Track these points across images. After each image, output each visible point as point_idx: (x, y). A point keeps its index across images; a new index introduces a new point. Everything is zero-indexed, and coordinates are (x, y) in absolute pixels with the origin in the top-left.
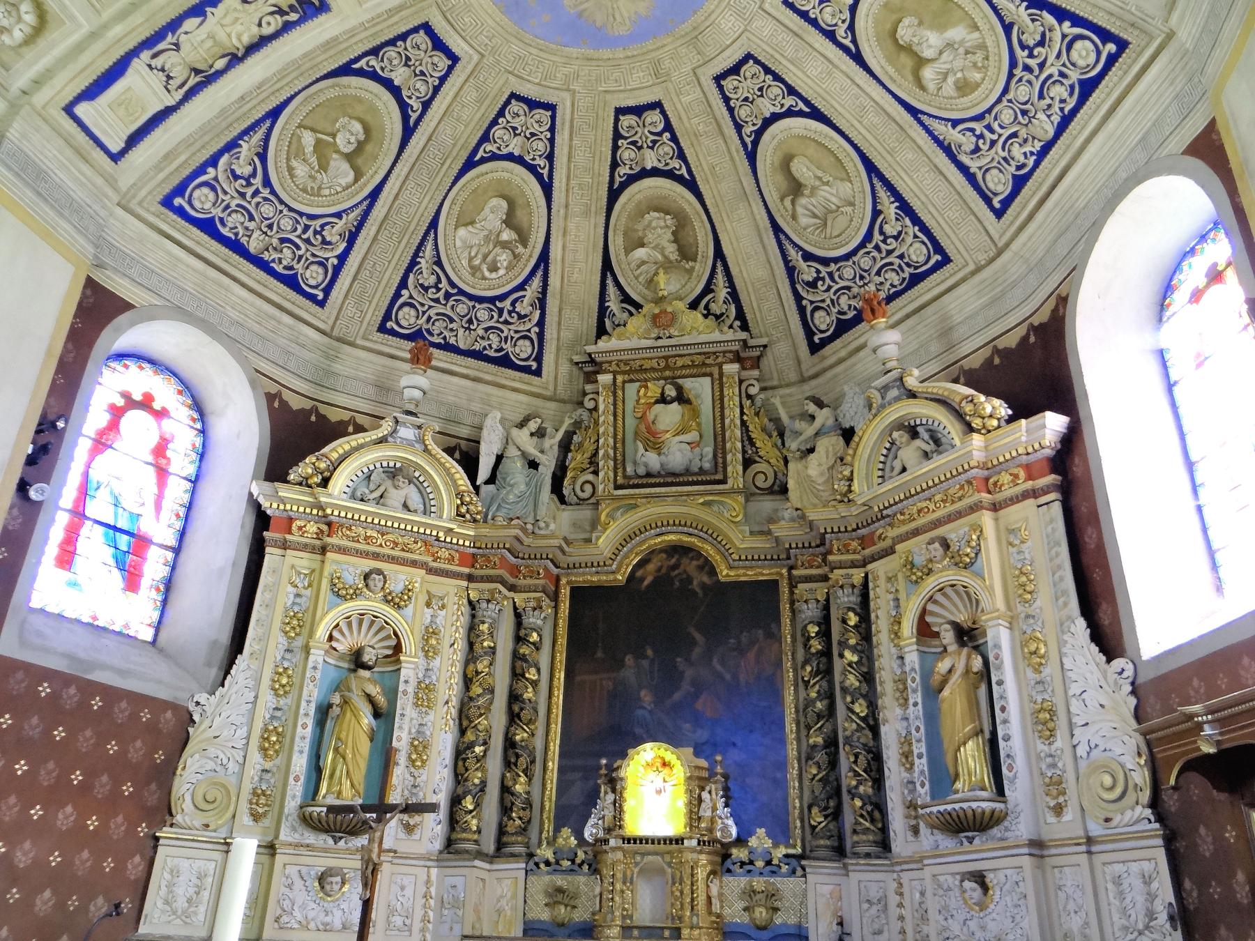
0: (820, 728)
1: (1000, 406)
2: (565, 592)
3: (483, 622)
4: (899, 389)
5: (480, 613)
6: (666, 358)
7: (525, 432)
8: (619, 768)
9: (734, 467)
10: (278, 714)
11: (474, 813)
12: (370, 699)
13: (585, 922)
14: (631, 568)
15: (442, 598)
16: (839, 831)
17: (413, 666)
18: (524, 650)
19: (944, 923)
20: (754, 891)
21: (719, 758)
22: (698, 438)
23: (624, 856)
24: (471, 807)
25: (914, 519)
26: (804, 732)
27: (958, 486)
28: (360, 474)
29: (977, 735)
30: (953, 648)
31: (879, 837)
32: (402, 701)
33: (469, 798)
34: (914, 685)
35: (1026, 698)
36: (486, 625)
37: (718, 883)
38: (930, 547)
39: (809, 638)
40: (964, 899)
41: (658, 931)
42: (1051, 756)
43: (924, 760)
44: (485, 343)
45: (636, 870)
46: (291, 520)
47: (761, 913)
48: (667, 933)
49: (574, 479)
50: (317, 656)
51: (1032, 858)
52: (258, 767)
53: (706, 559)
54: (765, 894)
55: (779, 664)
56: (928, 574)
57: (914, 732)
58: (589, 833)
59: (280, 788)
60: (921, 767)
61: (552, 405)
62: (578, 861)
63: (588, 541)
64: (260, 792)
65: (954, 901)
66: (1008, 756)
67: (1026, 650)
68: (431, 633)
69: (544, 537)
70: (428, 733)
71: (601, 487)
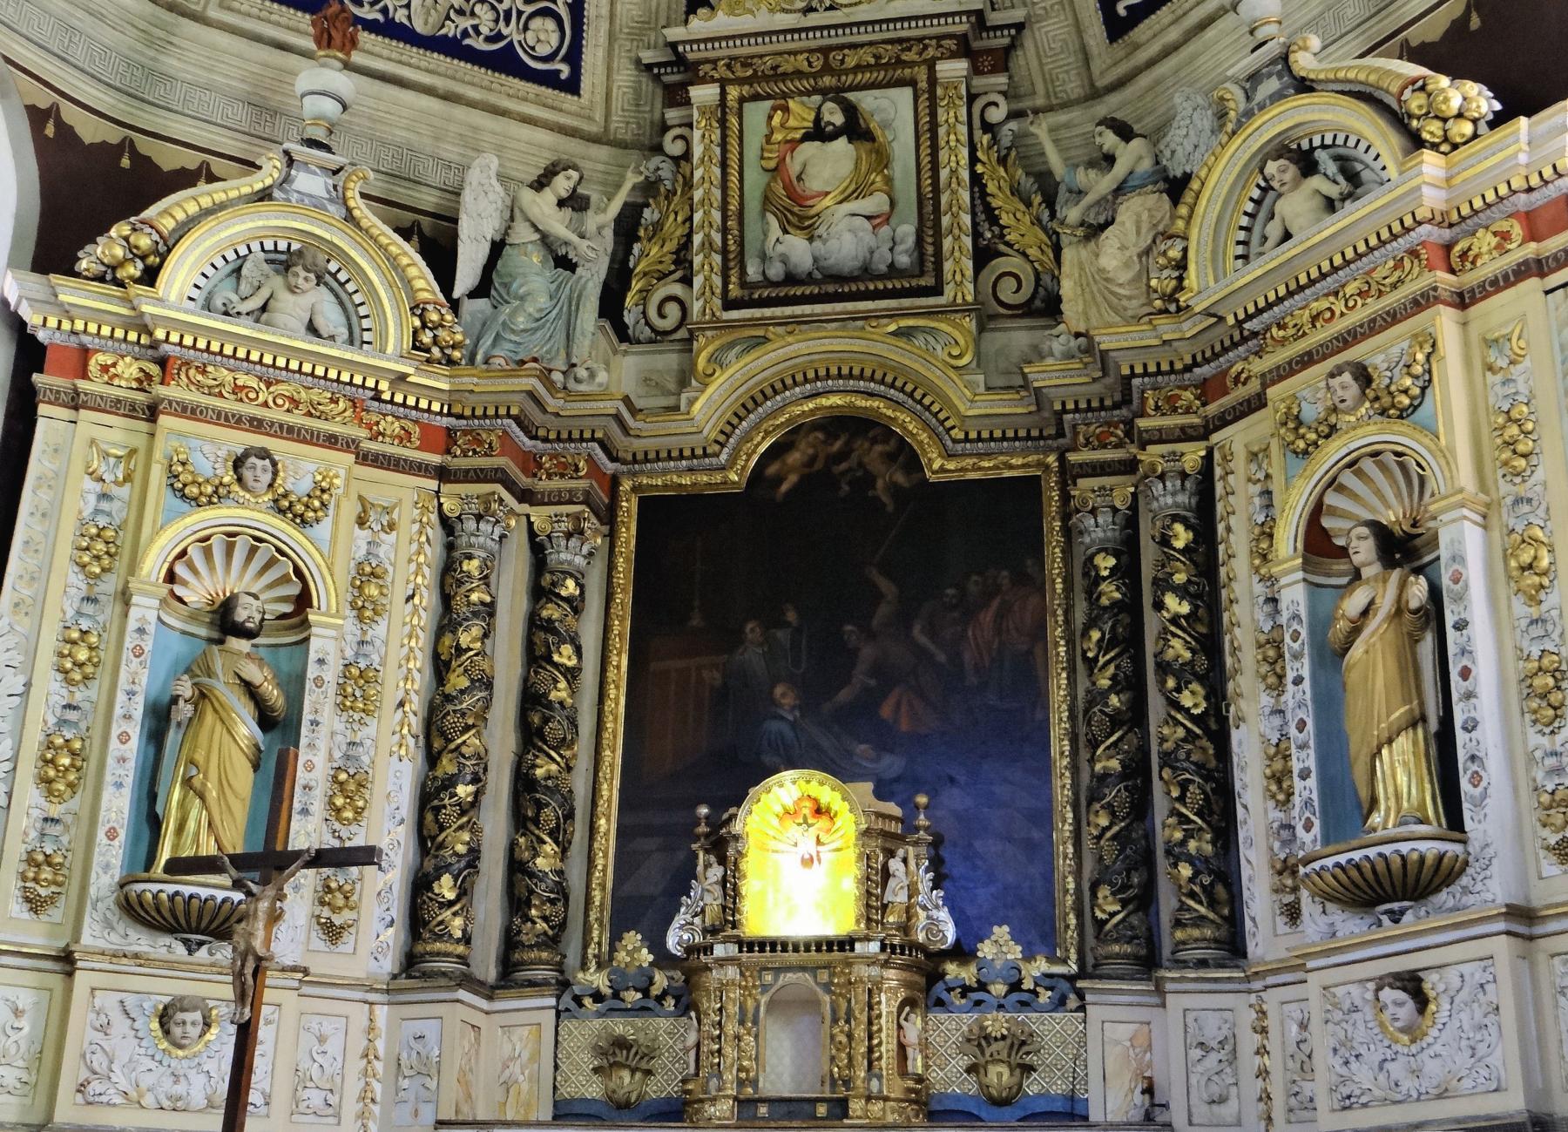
0: (1115, 744)
1: (1479, 94)
2: (629, 507)
3: (470, 557)
4: (1280, 76)
5: (464, 539)
6: (825, 51)
7: (549, 197)
8: (733, 817)
9: (957, 262)
10: (72, 715)
11: (457, 907)
12: (250, 690)
13: (669, 1099)
14: (755, 458)
15: (387, 510)
16: (1149, 929)
17: (333, 633)
18: (550, 611)
19: (1344, 1071)
20: (987, 1038)
21: (922, 800)
22: (886, 208)
23: (742, 974)
24: (450, 895)
25: (1305, 334)
26: (1084, 755)
27: (1391, 263)
28: (220, 263)
29: (1414, 725)
30: (1371, 571)
31: (1223, 933)
32: (314, 697)
33: (447, 880)
34: (1296, 646)
35: (1510, 654)
36: (475, 563)
37: (919, 1021)
38: (1335, 382)
39: (1099, 580)
40: (1382, 1025)
41: (806, 1107)
42: (1555, 754)
43: (1312, 782)
44: (466, 23)
45: (764, 1000)
46: (85, 353)
47: (1000, 1075)
48: (822, 1110)
49: (645, 293)
50: (145, 608)
51: (1512, 939)
52: (36, 813)
53: (902, 439)
54: (1009, 1041)
55: (1039, 633)
56: (1327, 437)
57: (1293, 732)
58: (674, 940)
59: (80, 855)
60: (1306, 794)
61: (602, 152)
62: (656, 991)
63: (676, 408)
64: (40, 858)
65: (1361, 1030)
66: (1473, 758)
67: (1513, 563)
68: (367, 574)
69: (586, 397)
70: (366, 759)
71: (697, 306)
